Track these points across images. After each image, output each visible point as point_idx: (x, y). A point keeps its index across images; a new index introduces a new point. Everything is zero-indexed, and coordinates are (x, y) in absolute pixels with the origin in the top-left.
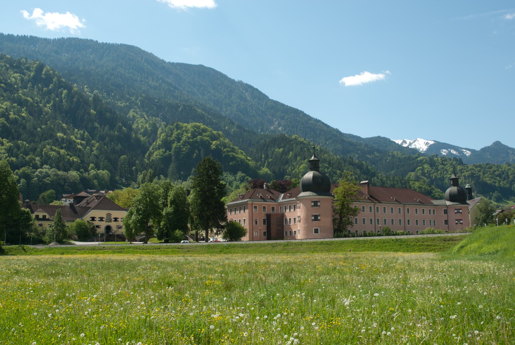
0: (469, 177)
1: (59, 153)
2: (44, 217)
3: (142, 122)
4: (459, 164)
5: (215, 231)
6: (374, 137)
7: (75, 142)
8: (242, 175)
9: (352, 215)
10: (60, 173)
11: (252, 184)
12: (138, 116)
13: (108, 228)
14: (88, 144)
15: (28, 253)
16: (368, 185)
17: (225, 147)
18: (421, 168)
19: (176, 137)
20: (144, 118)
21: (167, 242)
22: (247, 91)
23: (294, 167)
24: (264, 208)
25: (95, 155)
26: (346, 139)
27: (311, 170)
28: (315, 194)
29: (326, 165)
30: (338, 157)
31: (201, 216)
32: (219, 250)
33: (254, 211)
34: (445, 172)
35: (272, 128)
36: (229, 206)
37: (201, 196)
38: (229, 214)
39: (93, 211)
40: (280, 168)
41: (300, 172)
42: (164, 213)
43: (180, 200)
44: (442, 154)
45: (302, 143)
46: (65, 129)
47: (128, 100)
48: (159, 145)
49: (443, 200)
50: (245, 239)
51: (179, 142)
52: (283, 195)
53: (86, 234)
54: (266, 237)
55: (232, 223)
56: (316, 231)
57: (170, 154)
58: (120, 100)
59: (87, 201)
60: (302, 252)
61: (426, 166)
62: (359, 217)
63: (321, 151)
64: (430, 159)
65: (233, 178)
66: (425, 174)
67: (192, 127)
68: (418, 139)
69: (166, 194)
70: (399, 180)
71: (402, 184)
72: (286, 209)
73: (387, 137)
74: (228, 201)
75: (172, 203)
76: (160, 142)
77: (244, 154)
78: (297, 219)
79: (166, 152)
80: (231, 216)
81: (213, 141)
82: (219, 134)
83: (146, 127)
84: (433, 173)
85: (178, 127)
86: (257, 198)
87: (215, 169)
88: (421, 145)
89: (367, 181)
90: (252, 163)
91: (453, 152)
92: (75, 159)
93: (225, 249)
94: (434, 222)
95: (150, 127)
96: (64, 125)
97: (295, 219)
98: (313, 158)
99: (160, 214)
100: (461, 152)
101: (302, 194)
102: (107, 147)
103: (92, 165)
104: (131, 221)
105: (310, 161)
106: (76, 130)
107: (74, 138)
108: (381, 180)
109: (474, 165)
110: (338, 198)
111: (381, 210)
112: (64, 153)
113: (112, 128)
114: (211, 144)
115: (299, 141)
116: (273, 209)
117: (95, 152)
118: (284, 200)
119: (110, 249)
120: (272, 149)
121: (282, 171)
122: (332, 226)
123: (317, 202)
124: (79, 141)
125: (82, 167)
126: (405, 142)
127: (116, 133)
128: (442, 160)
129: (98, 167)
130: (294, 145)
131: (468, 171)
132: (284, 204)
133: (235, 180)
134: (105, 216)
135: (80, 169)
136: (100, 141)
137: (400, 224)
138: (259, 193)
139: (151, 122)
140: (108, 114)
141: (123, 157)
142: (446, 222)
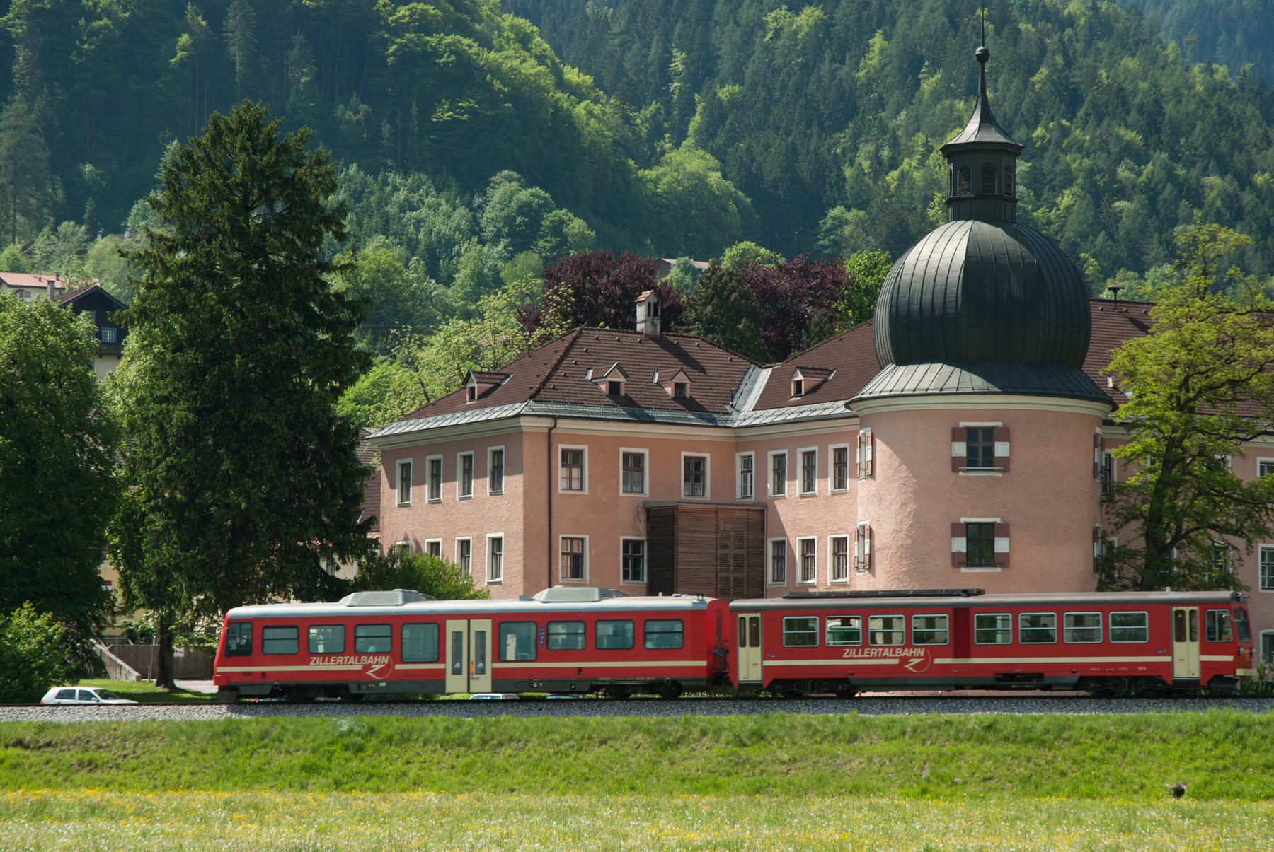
8: (524, 195)
9: (1237, 532)
23: (895, 144)
24: (633, 463)
27: (959, 209)
28: (978, 382)
29: (1129, 135)
30: (1221, 70)
31: (190, 521)
32: (300, 759)
33: (561, 484)
36: (392, 449)
37: (195, 375)
38: (390, 497)
40: (793, 152)
43: (49, 403)
60: (855, 790)
72: (779, 473)
74: (392, 398)
78: (855, 551)
86: (587, 395)
87: (297, 193)
90: (593, 115)
93: (340, 755)
97: (840, 544)
101: (895, 379)
105: (951, 152)
110: (1143, 412)
116: (695, 470)
118: (768, 416)
121: (805, 170)
132: (773, 443)
133: (475, 229)
138: (600, 362)
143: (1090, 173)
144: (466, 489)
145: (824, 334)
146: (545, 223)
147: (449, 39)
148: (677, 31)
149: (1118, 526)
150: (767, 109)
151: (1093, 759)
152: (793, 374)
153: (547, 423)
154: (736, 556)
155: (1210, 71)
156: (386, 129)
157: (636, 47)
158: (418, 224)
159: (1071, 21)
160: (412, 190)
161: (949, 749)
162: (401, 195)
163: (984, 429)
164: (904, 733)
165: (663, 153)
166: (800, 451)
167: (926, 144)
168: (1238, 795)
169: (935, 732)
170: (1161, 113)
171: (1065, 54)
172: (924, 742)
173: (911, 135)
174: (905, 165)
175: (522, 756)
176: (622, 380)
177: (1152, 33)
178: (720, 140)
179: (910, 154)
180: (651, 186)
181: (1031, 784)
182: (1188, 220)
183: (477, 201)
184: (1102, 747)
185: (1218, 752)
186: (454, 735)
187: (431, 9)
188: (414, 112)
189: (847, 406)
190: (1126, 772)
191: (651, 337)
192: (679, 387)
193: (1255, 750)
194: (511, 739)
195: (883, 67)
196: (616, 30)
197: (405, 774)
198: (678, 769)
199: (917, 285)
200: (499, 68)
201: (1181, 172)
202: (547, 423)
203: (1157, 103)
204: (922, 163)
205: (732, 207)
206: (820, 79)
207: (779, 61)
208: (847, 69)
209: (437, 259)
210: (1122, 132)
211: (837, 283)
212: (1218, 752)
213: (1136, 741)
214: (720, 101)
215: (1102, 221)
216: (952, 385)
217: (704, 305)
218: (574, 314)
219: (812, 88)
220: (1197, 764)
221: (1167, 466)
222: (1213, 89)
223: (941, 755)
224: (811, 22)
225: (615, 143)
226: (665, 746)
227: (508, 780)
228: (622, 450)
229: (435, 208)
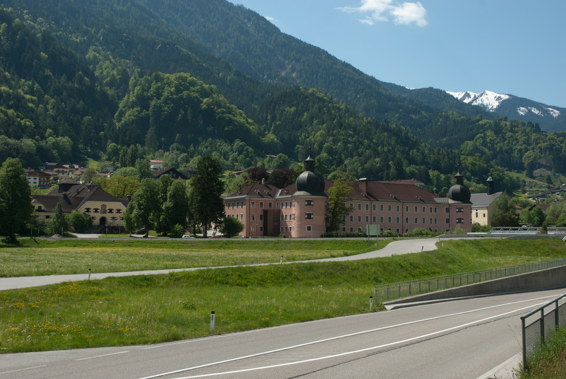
0: (546, 149)
1: (6, 114)
2: (40, 207)
3: (107, 67)
4: (535, 132)
5: (213, 225)
6: (424, 89)
7: (24, 98)
8: (241, 144)
10: (11, 141)
11: (251, 174)
12: (101, 57)
13: (103, 220)
14: (41, 100)
15: (40, 245)
16: (367, 183)
17: (219, 106)
18: (482, 135)
19: (154, 92)
20: (109, 59)
21: (165, 235)
22: (249, 20)
23: (309, 133)
24: (261, 204)
25: (52, 116)
26: (383, 92)
27: (307, 169)
28: (309, 194)
29: (351, 132)
32: (219, 245)
34: (514, 143)
35: (283, 74)
39: (88, 202)
41: (315, 141)
42: (163, 207)
44: (518, 113)
45: (321, 100)
46: (9, 80)
47: (86, 33)
48: (133, 102)
49: (447, 198)
50: (243, 234)
51: (159, 98)
52: (280, 190)
53: (84, 226)
54: (262, 232)
55: (230, 219)
56: (309, 229)
57: (147, 114)
58: (74, 32)
59: (78, 190)
61: (489, 133)
62: (354, 214)
63: (347, 110)
64: (496, 123)
65: (229, 147)
66: (487, 143)
67: (177, 79)
68: (487, 92)
69: (166, 188)
70: (445, 153)
71: (450, 159)
73: (442, 88)
75: (171, 196)
76: (134, 98)
77: (244, 115)
79: (141, 111)
80: (229, 211)
81: (203, 98)
82: (211, 89)
83: (113, 75)
84: (498, 143)
85: (158, 79)
88: (490, 100)
89: (365, 179)
90: (253, 128)
91: (535, 111)
92: (27, 123)
94: (436, 221)
95: (118, 75)
96: (7, 73)
97: (291, 215)
98: (308, 159)
99: (160, 209)
100: (547, 112)
101: (298, 193)
102: (65, 103)
103: (49, 131)
104: (133, 215)
106: (23, 80)
107: (22, 93)
108: (423, 153)
109: (556, 134)
111: (378, 208)
112: (13, 113)
113: (70, 78)
114: (201, 102)
115: (318, 97)
116: (270, 204)
117: (51, 112)
119: (120, 243)
120: (282, 108)
122: (324, 224)
123: (311, 201)
124: (28, 96)
125: (37, 132)
126: (468, 95)
127: (76, 85)
128: (511, 125)
129: (56, 133)
130: (311, 104)
131: (546, 142)
133: (232, 150)
134: (100, 207)
135: (35, 136)
136: (56, 96)
137: (398, 222)
139: (120, 68)
140: (64, 59)
141: (87, 118)
142: (448, 221)
143: (344, 139)
155: (367, 119)
158: (222, 149)
159: (342, 109)
162: (219, 144)
174: (310, 137)
178: (277, 132)
181: (311, 248)
201: (360, 139)
209: (225, 155)
215: (346, 148)
229: (225, 146)
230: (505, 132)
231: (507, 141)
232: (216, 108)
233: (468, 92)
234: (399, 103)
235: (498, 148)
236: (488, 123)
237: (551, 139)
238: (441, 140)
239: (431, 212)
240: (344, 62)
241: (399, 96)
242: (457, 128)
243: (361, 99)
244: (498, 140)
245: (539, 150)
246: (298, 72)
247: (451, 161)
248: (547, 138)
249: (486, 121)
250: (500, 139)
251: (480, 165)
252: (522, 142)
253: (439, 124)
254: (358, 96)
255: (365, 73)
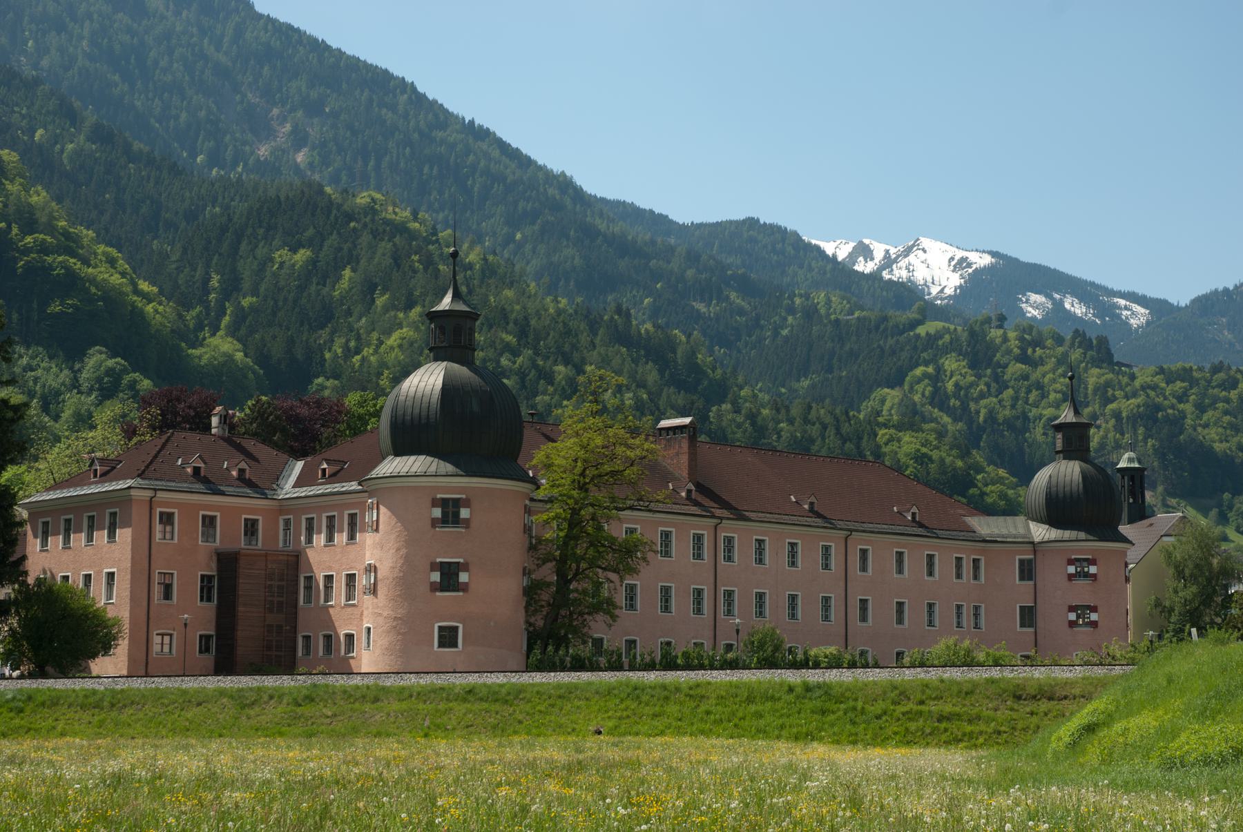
0: (1135, 419)
4: (1097, 362)
8: (110, 363)
9: (615, 571)
11: (155, 410)
16: (693, 439)
17: (30, 226)
18: (930, 369)
23: (358, 338)
24: (209, 522)
26: (602, 226)
28: (450, 468)
30: (563, 302)
33: (158, 535)
35: (263, 151)
36: (37, 511)
38: (33, 545)
41: (383, 365)
44: (1022, 313)
45: (400, 228)
49: (1020, 520)
50: (109, 667)
52: (300, 465)
54: (209, 659)
55: (50, 590)
56: (448, 638)
60: (378, 735)
61: (951, 363)
62: (646, 580)
64: (972, 333)
65: (65, 376)
68: (925, 242)
70: (828, 420)
77: (122, 264)
78: (362, 581)
80: (46, 559)
84: (982, 396)
88: (936, 269)
90: (159, 313)
94: (976, 615)
97: (351, 578)
98: (446, 303)
101: (392, 466)
105: (433, 316)
108: (752, 417)
109: (1161, 371)
110: (555, 491)
115: (387, 222)
116: (251, 528)
120: (261, 251)
121: (299, 353)
122: (521, 616)
123: (457, 503)
130: (365, 238)
133: (75, 385)
137: (826, 618)
144: (90, 539)
145: (330, 444)
146: (124, 382)
147: (60, 259)
148: (214, 261)
149: (539, 566)
150: (274, 314)
151: (540, 712)
152: (321, 464)
153: (149, 494)
154: (279, 587)
156: (15, 316)
157: (187, 270)
158: (36, 380)
159: (470, 266)
160: (32, 358)
161: (442, 706)
162: (25, 361)
163: (453, 500)
164: (411, 696)
165: (204, 339)
166: (324, 516)
167: (379, 339)
168: (637, 734)
169: (433, 695)
170: (528, 325)
171: (468, 286)
172: (425, 702)
173: (369, 333)
174: (365, 353)
175: (141, 715)
176: (202, 465)
177: (521, 276)
178: (243, 331)
179: (369, 345)
180: (197, 360)
182: (545, 393)
183: (77, 366)
184: (546, 704)
185: (623, 706)
186: (91, 700)
187: (49, 239)
188: (35, 306)
189: (360, 484)
190: (563, 720)
191: (222, 438)
192: (242, 471)
193: (647, 704)
194: (132, 703)
195: (351, 289)
196: (174, 258)
197: (54, 728)
198: (253, 722)
199: (409, 403)
200: (94, 279)
202: (149, 494)
203: (526, 318)
204: (376, 352)
205: (251, 375)
206: (309, 295)
207: (282, 283)
208: (327, 289)
209: (50, 402)
210: (504, 336)
211: (339, 412)
212: (623, 706)
213: (569, 700)
214: (243, 308)
216: (433, 469)
217: (251, 423)
218: (161, 428)
219: (304, 301)
220: (610, 714)
221: (571, 526)
222: (559, 312)
223: (437, 711)
224: (304, 258)
225: (173, 331)
226: (243, 707)
227: (131, 731)
228: (201, 513)
230: (1004, 360)
231: (1010, 391)
232: (15, 230)
233: (866, 241)
234: (653, 263)
235: (983, 412)
236: (948, 331)
237: (1150, 387)
238: (796, 385)
239: (959, 576)
240: (472, 122)
241: (653, 242)
242: (847, 347)
243: (528, 247)
244: (982, 387)
245: (1113, 422)
246: (313, 148)
247: (848, 445)
248: (1137, 383)
249: (939, 325)
250: (988, 385)
251: (942, 460)
252: (1059, 396)
253: (785, 332)
254: (518, 236)
255: (540, 162)
